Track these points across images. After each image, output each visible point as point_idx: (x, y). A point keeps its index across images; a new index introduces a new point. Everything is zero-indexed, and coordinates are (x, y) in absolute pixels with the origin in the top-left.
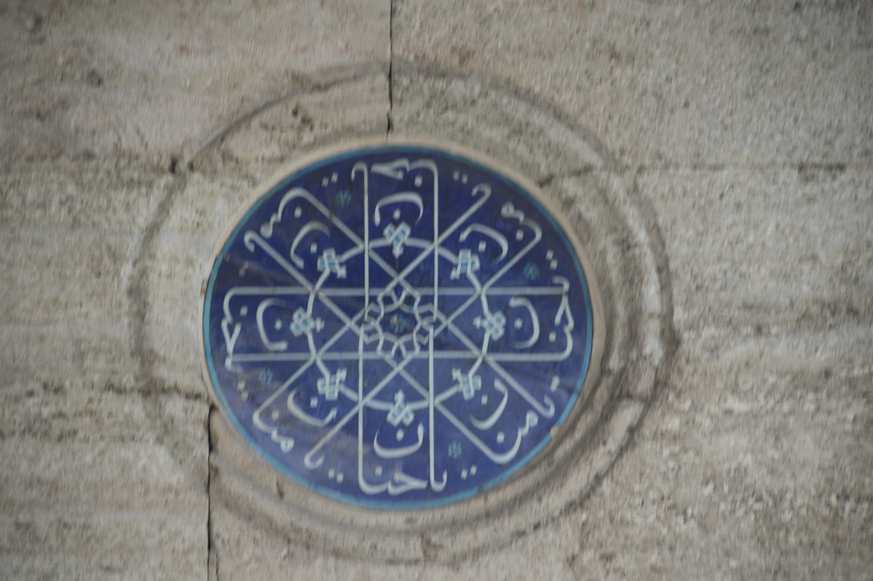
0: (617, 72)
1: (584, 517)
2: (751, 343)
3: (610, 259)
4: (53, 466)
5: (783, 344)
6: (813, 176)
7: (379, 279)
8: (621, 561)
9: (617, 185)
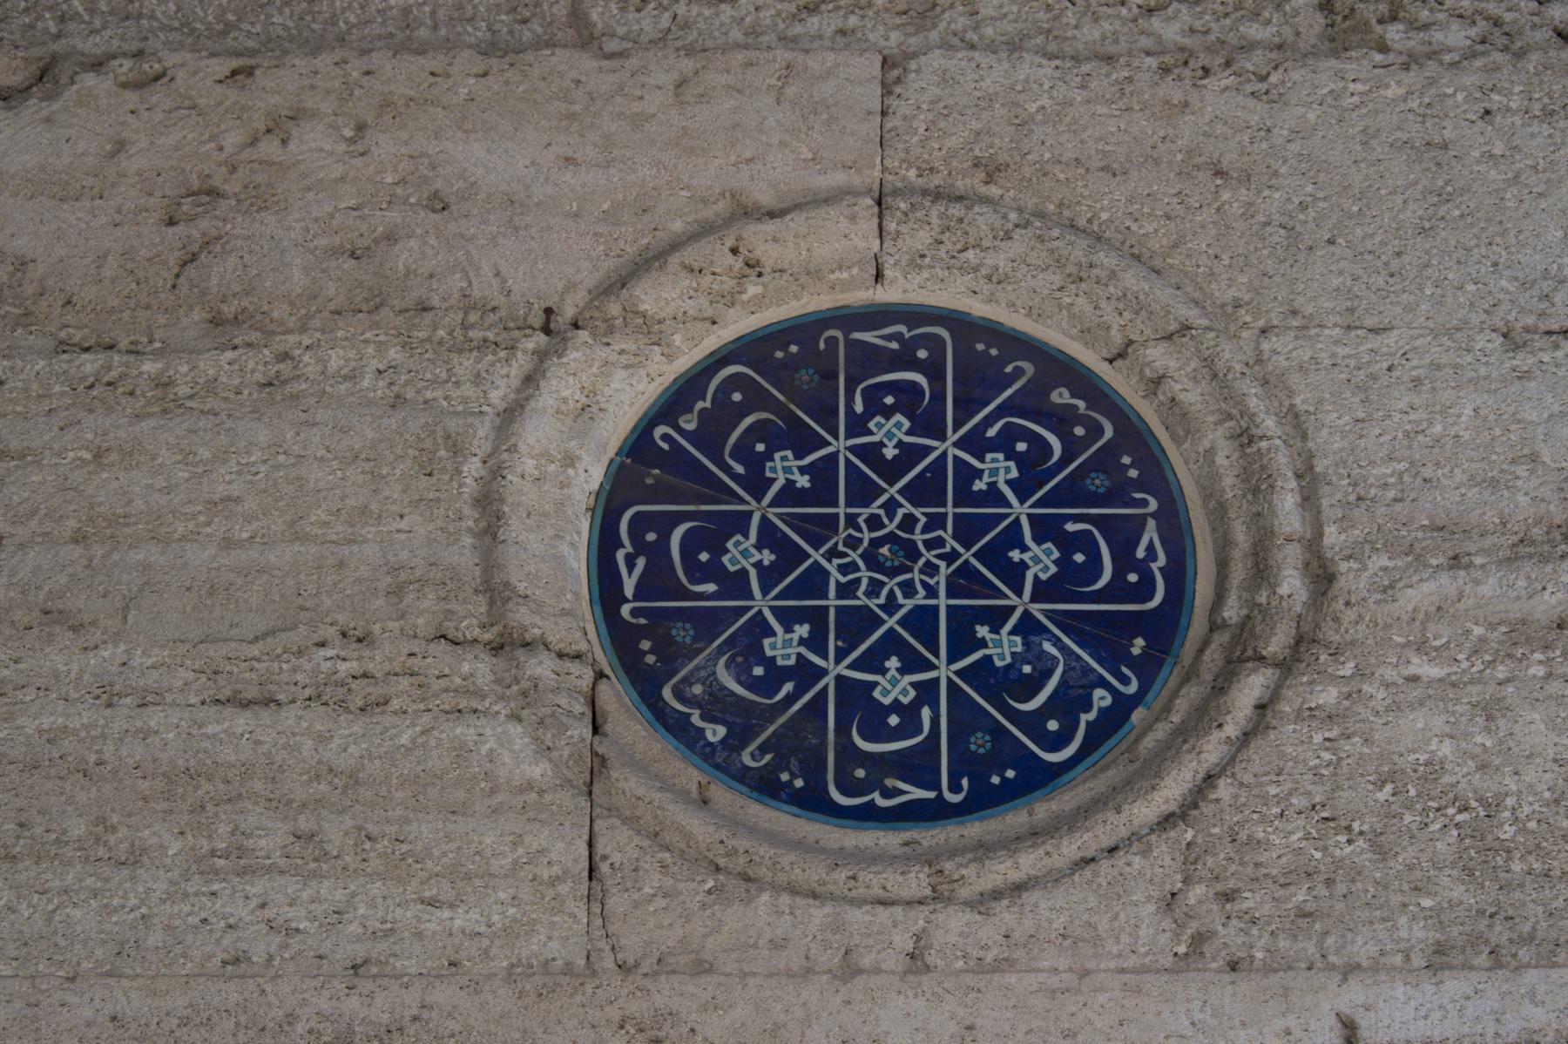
0: (1226, 196)
1: (1189, 835)
2: (1444, 578)
3: (1220, 460)
4: (352, 749)
5: (1492, 580)
6: (1525, 343)
7: (862, 492)
8: (1249, 901)
9: (1231, 355)
